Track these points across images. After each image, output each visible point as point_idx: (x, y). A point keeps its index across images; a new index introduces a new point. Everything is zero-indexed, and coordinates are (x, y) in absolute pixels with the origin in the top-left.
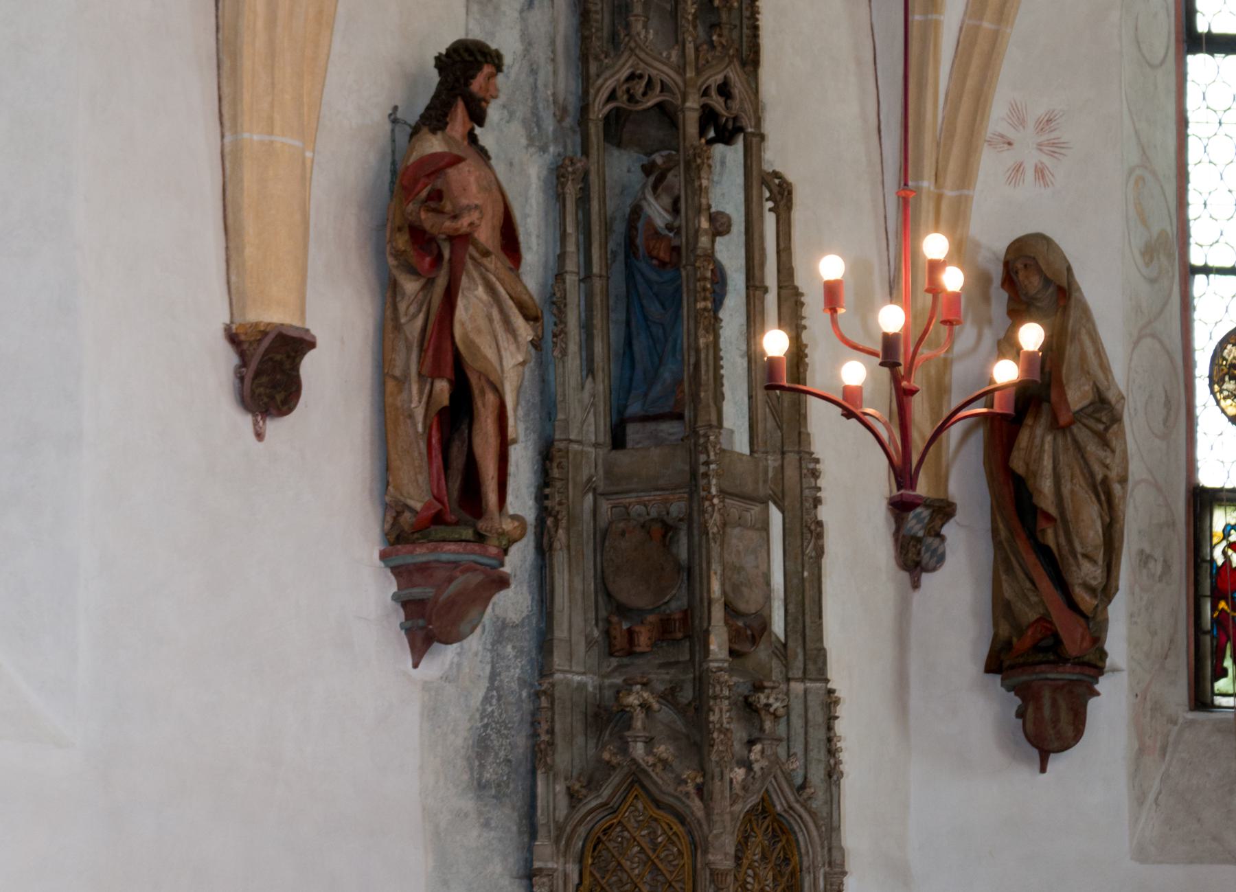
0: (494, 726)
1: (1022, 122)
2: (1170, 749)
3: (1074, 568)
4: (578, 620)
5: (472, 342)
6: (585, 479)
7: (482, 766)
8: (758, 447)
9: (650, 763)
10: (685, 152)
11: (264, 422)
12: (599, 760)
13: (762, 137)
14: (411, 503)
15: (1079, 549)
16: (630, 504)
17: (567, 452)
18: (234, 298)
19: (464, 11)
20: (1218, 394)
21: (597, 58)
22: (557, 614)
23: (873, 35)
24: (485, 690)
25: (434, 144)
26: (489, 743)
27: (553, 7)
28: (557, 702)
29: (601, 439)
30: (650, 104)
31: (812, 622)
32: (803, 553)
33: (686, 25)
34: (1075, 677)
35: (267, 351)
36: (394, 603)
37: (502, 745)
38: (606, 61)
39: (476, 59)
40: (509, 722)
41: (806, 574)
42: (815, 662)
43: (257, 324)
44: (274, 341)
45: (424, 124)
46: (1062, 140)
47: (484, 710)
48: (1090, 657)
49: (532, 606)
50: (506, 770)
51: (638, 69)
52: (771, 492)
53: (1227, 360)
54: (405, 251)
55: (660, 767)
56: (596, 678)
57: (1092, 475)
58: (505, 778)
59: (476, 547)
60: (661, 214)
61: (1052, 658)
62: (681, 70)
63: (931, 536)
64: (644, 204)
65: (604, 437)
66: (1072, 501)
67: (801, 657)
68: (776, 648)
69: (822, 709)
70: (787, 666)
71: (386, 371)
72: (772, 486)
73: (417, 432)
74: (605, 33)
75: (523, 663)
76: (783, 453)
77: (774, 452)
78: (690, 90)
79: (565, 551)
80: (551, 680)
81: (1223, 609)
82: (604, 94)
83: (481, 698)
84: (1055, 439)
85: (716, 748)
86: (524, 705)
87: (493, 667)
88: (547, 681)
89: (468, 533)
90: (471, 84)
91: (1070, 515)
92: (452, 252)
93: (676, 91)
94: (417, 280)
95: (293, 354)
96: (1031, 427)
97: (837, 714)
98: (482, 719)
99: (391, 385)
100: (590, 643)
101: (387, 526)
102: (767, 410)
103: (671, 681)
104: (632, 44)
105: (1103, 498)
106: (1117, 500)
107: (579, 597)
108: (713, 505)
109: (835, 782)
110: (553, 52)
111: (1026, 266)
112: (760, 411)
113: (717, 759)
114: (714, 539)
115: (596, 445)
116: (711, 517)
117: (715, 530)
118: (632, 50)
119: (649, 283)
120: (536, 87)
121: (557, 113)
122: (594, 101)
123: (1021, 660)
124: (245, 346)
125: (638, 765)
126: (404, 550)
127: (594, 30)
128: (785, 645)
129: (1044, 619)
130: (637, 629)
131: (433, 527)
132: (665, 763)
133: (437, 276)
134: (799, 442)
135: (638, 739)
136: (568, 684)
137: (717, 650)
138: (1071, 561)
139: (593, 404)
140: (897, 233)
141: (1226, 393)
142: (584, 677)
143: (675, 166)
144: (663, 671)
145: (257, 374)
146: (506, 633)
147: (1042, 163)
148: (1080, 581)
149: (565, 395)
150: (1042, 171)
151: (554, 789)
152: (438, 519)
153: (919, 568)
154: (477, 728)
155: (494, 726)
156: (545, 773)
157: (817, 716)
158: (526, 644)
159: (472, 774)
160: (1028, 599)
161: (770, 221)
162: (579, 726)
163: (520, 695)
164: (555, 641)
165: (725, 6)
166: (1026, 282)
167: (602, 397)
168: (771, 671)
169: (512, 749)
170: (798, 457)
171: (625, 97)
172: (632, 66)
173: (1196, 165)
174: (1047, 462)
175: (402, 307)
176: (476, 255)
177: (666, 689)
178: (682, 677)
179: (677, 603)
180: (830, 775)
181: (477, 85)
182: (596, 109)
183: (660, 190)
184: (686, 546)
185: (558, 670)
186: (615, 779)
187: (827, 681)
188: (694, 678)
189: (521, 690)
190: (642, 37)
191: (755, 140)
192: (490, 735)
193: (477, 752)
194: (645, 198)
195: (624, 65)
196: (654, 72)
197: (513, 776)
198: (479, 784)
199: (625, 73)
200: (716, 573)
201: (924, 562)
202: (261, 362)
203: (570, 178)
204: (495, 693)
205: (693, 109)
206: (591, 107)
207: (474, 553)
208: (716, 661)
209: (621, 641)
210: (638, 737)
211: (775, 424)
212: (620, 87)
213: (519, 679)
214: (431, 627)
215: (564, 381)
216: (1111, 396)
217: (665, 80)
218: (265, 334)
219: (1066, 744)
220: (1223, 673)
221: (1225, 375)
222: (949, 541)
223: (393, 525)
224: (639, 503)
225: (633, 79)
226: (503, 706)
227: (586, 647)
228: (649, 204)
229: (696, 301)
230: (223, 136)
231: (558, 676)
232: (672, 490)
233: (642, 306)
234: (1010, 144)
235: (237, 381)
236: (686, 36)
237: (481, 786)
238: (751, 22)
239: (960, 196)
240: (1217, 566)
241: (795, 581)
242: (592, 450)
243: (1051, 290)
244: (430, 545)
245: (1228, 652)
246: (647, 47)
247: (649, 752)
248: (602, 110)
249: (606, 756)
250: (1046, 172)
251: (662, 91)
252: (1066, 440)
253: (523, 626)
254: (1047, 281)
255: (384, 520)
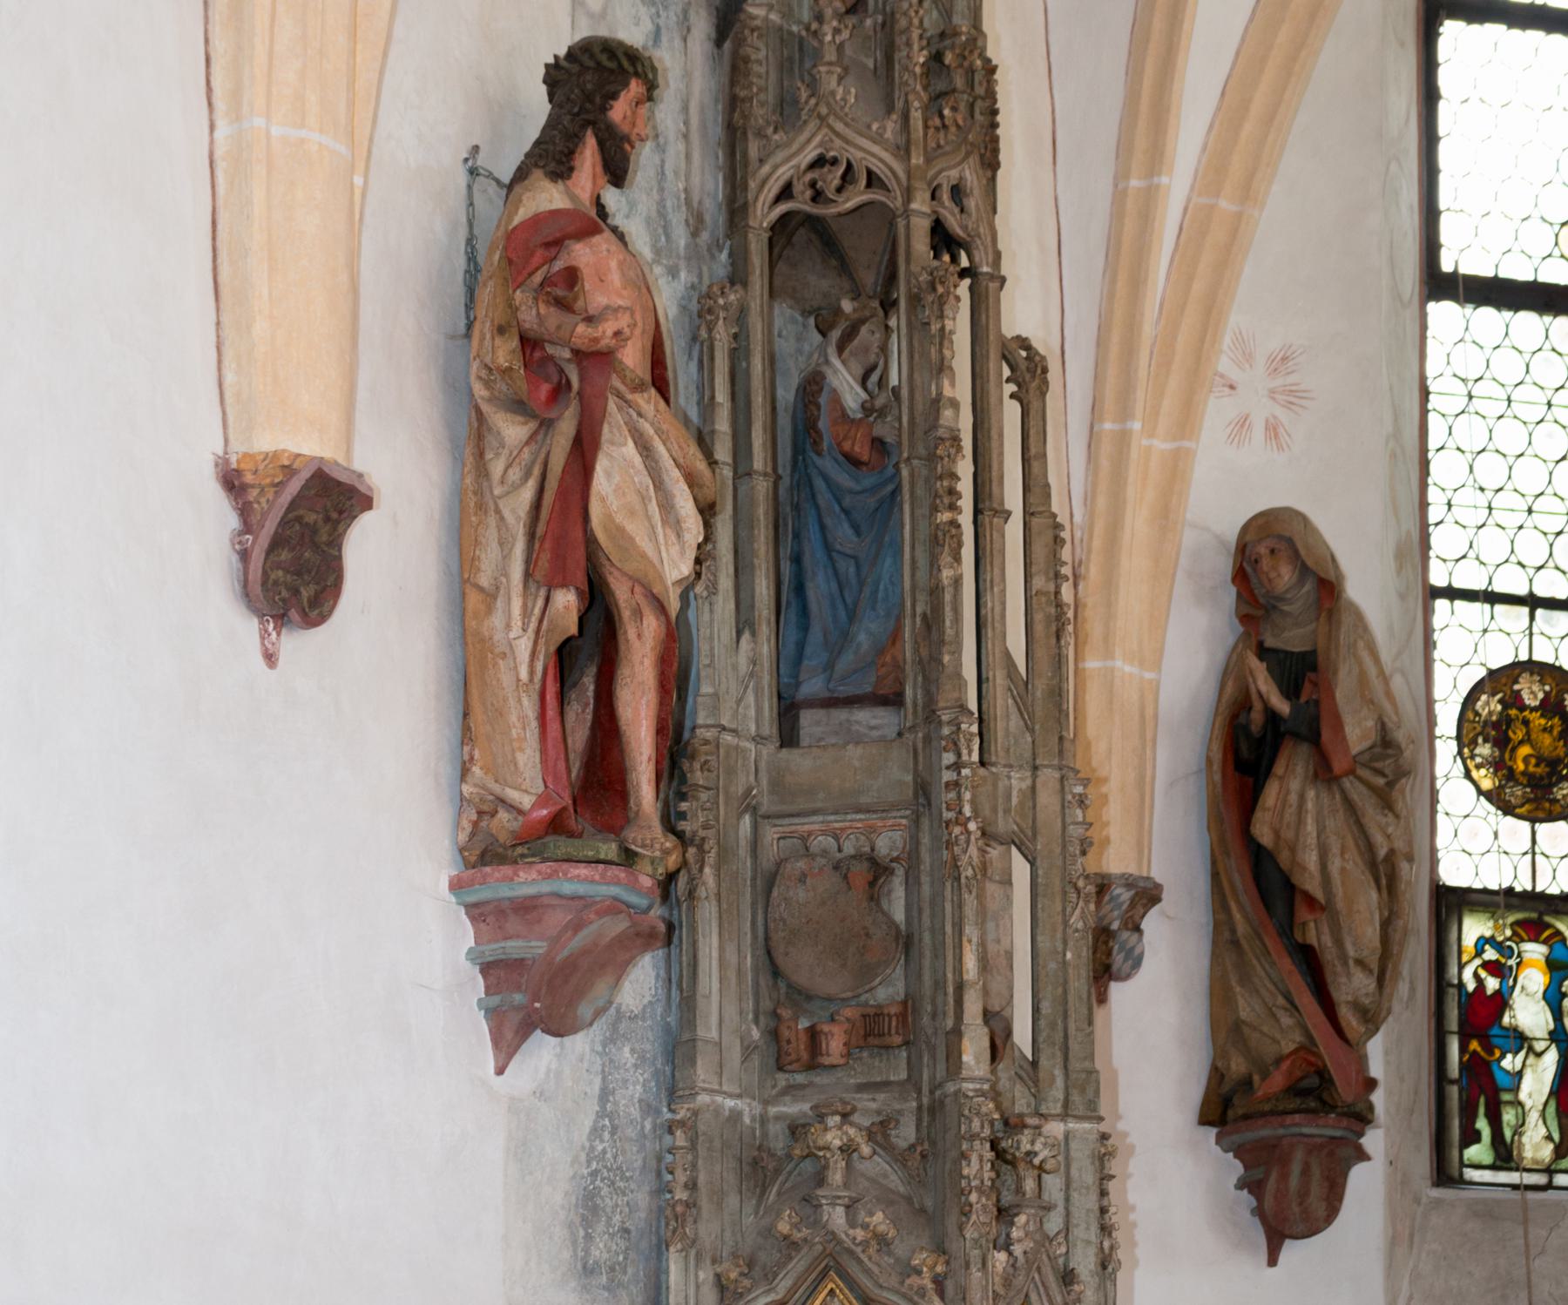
0: (606, 1174)
1: (1249, 357)
2: (1416, 1239)
3: (1343, 980)
4: (731, 1011)
5: (621, 530)
6: (740, 791)
7: (588, 1237)
8: (997, 756)
9: (859, 1239)
10: (908, 282)
11: (279, 634)
12: (768, 1232)
13: (1003, 280)
14: (513, 795)
15: (1351, 951)
16: (810, 833)
17: (718, 747)
18: (229, 410)
19: (568, 21)
20: (1468, 761)
21: (760, 134)
22: (701, 1002)
23: (1057, 213)
24: (594, 1117)
25: (547, 197)
26: (599, 1201)
27: (686, 54)
28: (701, 1139)
29: (766, 731)
30: (849, 205)
31: (1077, 1030)
32: (1066, 923)
33: (911, 82)
34: (1338, 1133)
35: (293, 505)
36: (468, 964)
37: (617, 1205)
38: (776, 137)
39: (620, 66)
40: (628, 1170)
41: (1069, 955)
42: (1083, 1091)
43: (276, 455)
44: (306, 486)
45: (536, 166)
46: (1302, 387)
47: (592, 1148)
48: (1360, 1107)
49: (656, 988)
50: (623, 1244)
51: (832, 149)
52: (1015, 828)
53: (1480, 715)
54: (510, 369)
55: (874, 1246)
56: (755, 1104)
57: (1370, 847)
58: (621, 1258)
59: (620, 873)
60: (852, 388)
61: (1313, 1104)
62: (903, 150)
63: (1127, 929)
64: (828, 372)
65: (769, 728)
66: (1343, 883)
67: (1060, 1082)
68: (1021, 1067)
69: (1093, 1163)
70: (1037, 1097)
71: (466, 576)
72: (1018, 819)
73: (519, 680)
74: (771, 96)
75: (646, 1076)
76: (1035, 768)
77: (1021, 767)
78: (917, 184)
79: (714, 903)
80: (692, 1106)
81: (1475, 1052)
82: (773, 188)
83: (587, 1130)
84: (1317, 796)
85: (974, 1217)
86: (648, 1144)
87: (604, 1079)
88: (686, 1106)
89: (609, 850)
90: (611, 107)
91: (1340, 904)
92: (582, 380)
93: (892, 184)
94: (525, 423)
95: (335, 515)
96: (1281, 778)
97: (1111, 1173)
98: (589, 1163)
99: (473, 599)
100: (748, 1051)
101: (463, 837)
102: (1010, 701)
103: (879, 1112)
104: (824, 110)
105: (1384, 882)
106: (1403, 886)
107: (732, 975)
108: (968, 833)
109: (1110, 1274)
110: (686, 123)
111: (1272, 551)
112: (1000, 702)
113: (976, 1235)
114: (968, 887)
115: (759, 739)
116: (965, 852)
117: (970, 872)
118: (822, 118)
119: (836, 492)
120: (663, 173)
121: (691, 222)
122: (757, 198)
123: (1267, 1107)
124: (253, 494)
125: (840, 1242)
126: (497, 875)
127: (755, 90)
128: (1034, 1064)
129: (1308, 1048)
130: (826, 1028)
131: (548, 839)
132: (883, 1241)
133: (558, 418)
134: (1061, 752)
135: (839, 1201)
136: (717, 1111)
137: (972, 1063)
138: (1339, 969)
139: (752, 675)
140: (1086, 499)
141: (1478, 760)
142: (738, 1102)
143: (871, 317)
144: (865, 1096)
145: (276, 544)
146: (623, 1027)
147: (1275, 417)
148: (1350, 998)
149: (713, 656)
150: (1275, 429)
151: (697, 1276)
152: (556, 825)
153: (1107, 976)
154: (583, 1177)
155: (606, 1174)
156: (682, 1251)
157: (1084, 1173)
158: (648, 1047)
159: (575, 1251)
160: (1277, 1020)
161: (1011, 413)
162: (731, 1179)
163: (643, 1127)
164: (699, 1044)
165: (961, 66)
166: (1273, 575)
167: (766, 665)
168: (1014, 1103)
169: (630, 1212)
170: (1057, 775)
171: (809, 193)
172: (821, 144)
173: (1438, 450)
174: (1310, 827)
175: (497, 468)
176: (622, 388)
177: (873, 1124)
178: (897, 1107)
179: (888, 991)
180: (1104, 1266)
181: (618, 111)
182: (759, 213)
183: (847, 352)
184: (903, 902)
185: (704, 1090)
186: (798, 1264)
187: (1101, 1119)
188: (920, 1108)
189: (643, 1119)
190: (838, 97)
191: (993, 286)
192: (600, 1189)
193: (583, 1215)
194: (827, 362)
195: (809, 141)
196: (855, 155)
197: (632, 1255)
198: (584, 1267)
199: (810, 155)
200: (970, 941)
201: (1115, 968)
202: (284, 523)
203: (722, 315)
204: (607, 1122)
205: (924, 213)
206: (751, 210)
207: (618, 883)
208: (972, 1080)
209: (800, 1048)
210: (839, 1197)
211: (1022, 723)
212: (799, 179)
213: (640, 1101)
214: (537, 1005)
215: (712, 633)
216: (1400, 736)
217: (874, 169)
218: (289, 471)
219: (1312, 1226)
220: (1475, 1137)
221: (1478, 735)
222: (1147, 937)
223: (473, 835)
224: (824, 833)
225: (822, 166)
226: (618, 1144)
227: (743, 1055)
228: (836, 371)
229: (935, 509)
230: (212, 127)
231: (703, 1099)
232: (883, 811)
233: (823, 527)
234: (1232, 387)
235: (235, 558)
236: (911, 97)
237: (588, 1270)
238: (987, 103)
239: (1178, 450)
240: (1467, 993)
241: (1052, 966)
242: (751, 746)
243: (1308, 587)
244: (546, 867)
245: (1482, 1110)
246: (846, 115)
247: (852, 1223)
248: (768, 213)
249: (784, 1227)
250: (1281, 430)
251: (869, 185)
252: (1334, 798)
253: (644, 1019)
254: (1304, 570)
255: (457, 825)
